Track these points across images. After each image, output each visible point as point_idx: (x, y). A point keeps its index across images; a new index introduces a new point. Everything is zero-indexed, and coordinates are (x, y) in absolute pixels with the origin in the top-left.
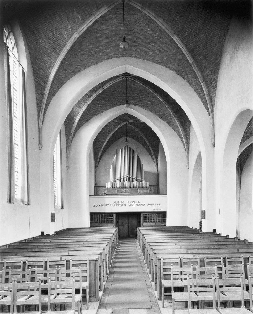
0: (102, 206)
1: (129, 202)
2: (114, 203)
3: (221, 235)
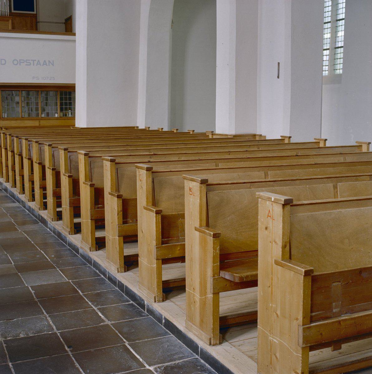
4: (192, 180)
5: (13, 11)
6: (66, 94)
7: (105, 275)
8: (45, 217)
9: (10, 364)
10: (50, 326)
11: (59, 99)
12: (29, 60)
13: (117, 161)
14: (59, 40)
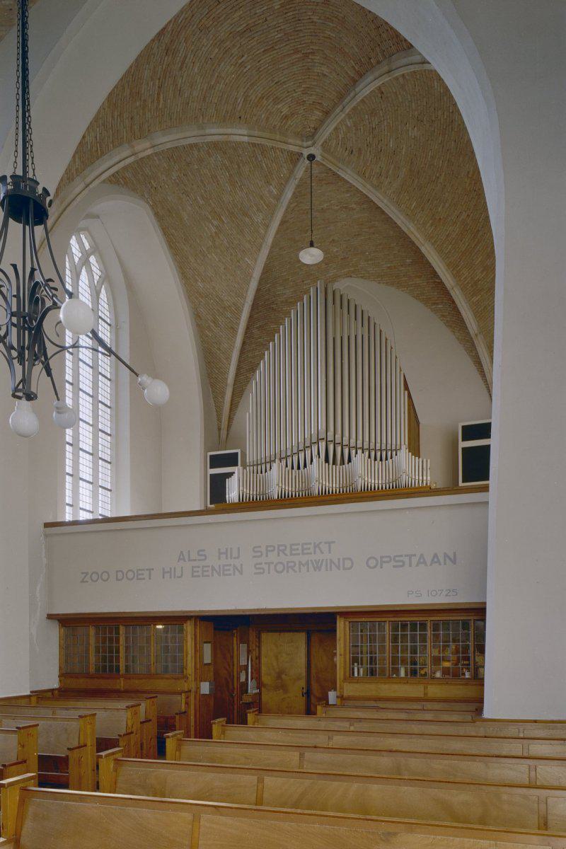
0: (120, 577)
1: (263, 550)
2: (181, 558)
5: (209, 505)
12: (401, 556)
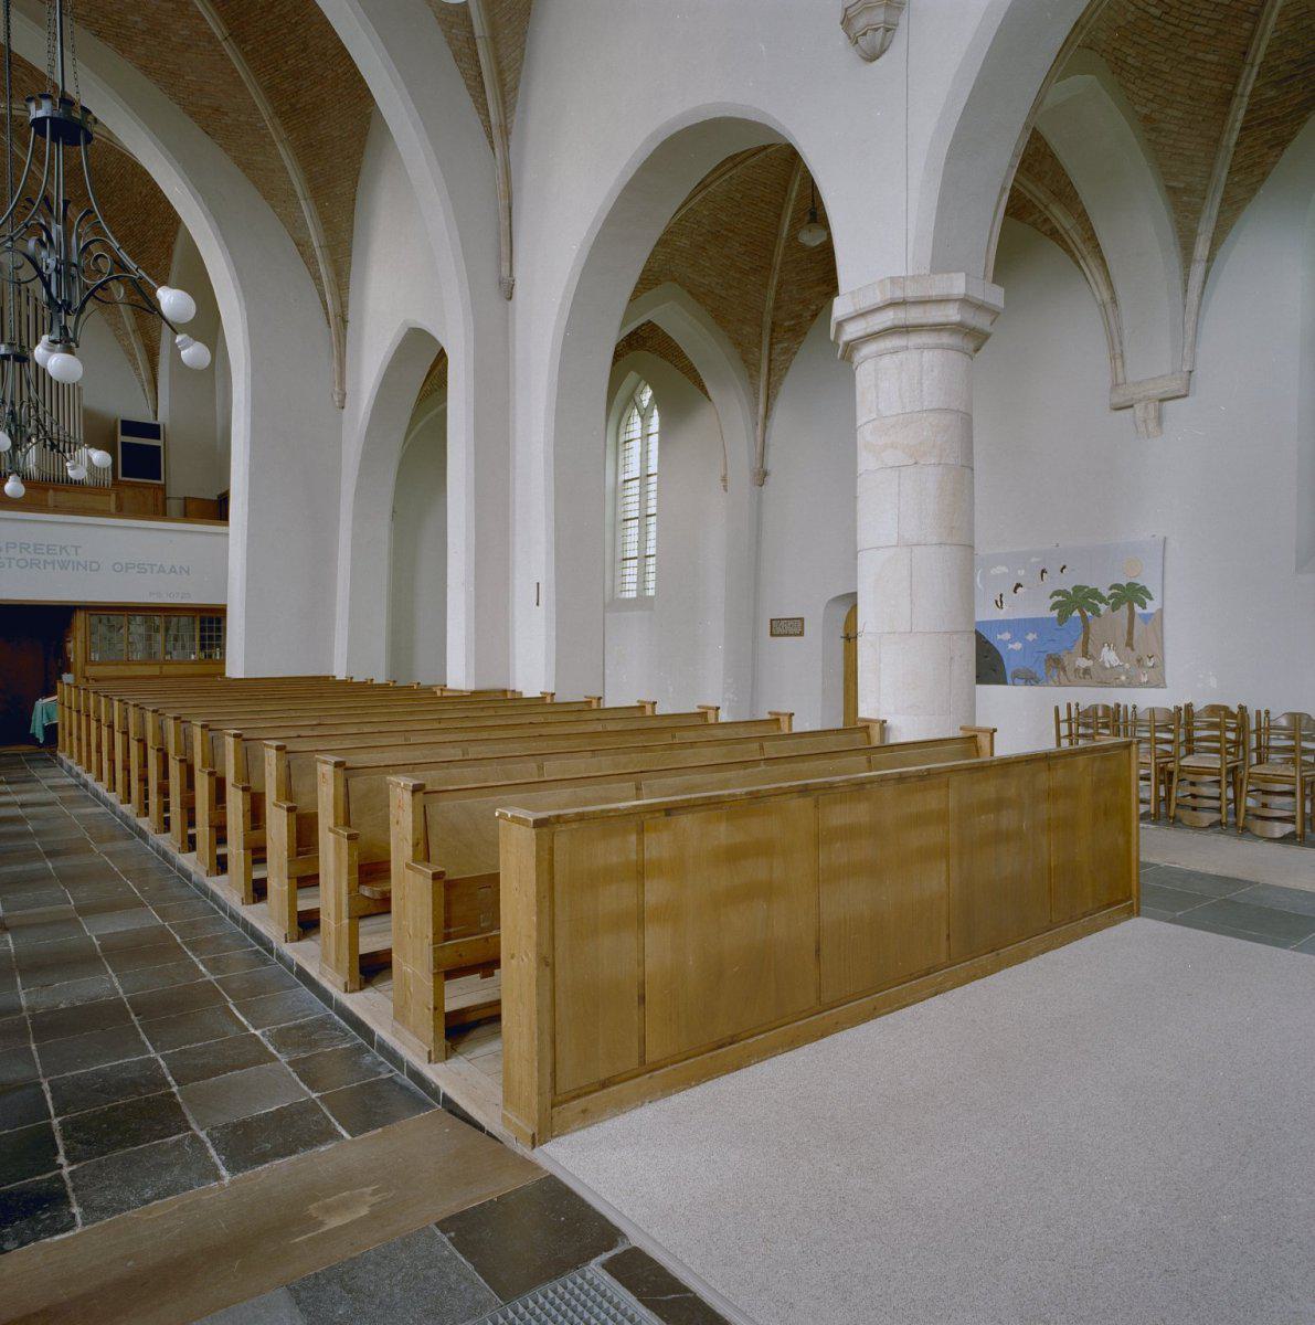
3: (552, 699)
4: (326, 762)
6: (211, 622)
7: (225, 912)
8: (145, 828)
9: (33, 1047)
10: (114, 988)
11: (198, 631)
13: (245, 736)
14: (206, 533)
